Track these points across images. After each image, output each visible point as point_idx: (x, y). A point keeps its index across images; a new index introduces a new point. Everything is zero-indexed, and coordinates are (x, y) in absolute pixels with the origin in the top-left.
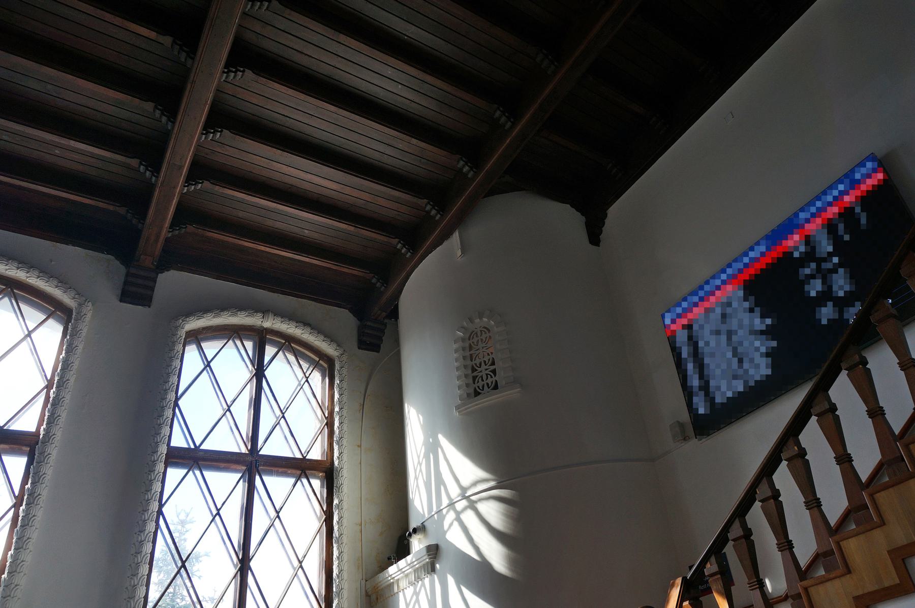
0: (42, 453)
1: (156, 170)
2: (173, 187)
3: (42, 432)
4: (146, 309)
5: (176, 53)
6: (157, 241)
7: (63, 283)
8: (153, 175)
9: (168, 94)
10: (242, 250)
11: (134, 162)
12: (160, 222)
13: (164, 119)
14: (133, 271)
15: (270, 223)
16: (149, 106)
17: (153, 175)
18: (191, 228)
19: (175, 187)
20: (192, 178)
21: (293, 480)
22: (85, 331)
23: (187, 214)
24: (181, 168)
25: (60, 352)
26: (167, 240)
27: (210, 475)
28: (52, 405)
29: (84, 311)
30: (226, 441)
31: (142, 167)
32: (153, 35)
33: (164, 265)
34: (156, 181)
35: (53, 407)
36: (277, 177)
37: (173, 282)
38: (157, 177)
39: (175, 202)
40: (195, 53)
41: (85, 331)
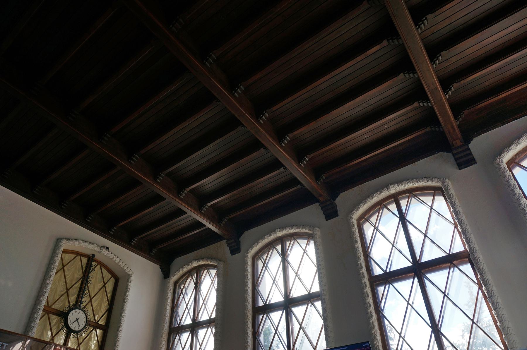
0: (475, 259)
1: (427, 99)
2: (440, 100)
3: (468, 249)
4: (475, 165)
5: (392, 43)
6: (454, 130)
7: (429, 178)
8: (428, 103)
9: (404, 64)
10: (504, 100)
11: (416, 104)
12: (449, 122)
13: (411, 75)
14: (455, 152)
15: (509, 73)
16: (401, 76)
17: (428, 103)
18: (466, 112)
19: (441, 99)
20: (445, 87)
21: (447, 271)
22: (454, 193)
23: (457, 107)
24: (436, 88)
25: (450, 209)
26: (459, 126)
27: (397, 285)
28: (463, 234)
29: (446, 184)
30: (402, 262)
31: (421, 104)
32: (378, 47)
33: (467, 140)
34: (431, 104)
35: (464, 234)
36: (490, 47)
37: (479, 144)
38: (430, 102)
39: (447, 106)
40: (398, 35)
41: (454, 193)
